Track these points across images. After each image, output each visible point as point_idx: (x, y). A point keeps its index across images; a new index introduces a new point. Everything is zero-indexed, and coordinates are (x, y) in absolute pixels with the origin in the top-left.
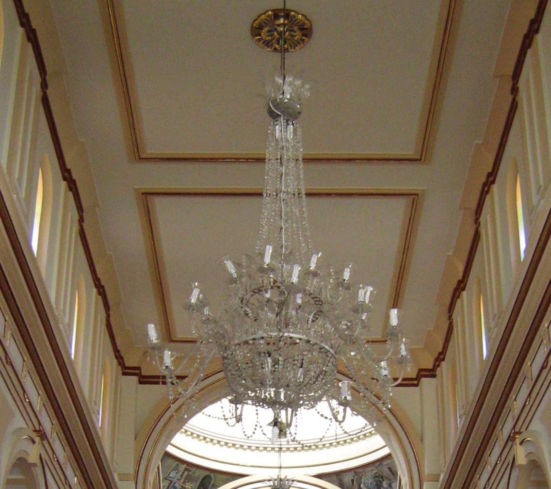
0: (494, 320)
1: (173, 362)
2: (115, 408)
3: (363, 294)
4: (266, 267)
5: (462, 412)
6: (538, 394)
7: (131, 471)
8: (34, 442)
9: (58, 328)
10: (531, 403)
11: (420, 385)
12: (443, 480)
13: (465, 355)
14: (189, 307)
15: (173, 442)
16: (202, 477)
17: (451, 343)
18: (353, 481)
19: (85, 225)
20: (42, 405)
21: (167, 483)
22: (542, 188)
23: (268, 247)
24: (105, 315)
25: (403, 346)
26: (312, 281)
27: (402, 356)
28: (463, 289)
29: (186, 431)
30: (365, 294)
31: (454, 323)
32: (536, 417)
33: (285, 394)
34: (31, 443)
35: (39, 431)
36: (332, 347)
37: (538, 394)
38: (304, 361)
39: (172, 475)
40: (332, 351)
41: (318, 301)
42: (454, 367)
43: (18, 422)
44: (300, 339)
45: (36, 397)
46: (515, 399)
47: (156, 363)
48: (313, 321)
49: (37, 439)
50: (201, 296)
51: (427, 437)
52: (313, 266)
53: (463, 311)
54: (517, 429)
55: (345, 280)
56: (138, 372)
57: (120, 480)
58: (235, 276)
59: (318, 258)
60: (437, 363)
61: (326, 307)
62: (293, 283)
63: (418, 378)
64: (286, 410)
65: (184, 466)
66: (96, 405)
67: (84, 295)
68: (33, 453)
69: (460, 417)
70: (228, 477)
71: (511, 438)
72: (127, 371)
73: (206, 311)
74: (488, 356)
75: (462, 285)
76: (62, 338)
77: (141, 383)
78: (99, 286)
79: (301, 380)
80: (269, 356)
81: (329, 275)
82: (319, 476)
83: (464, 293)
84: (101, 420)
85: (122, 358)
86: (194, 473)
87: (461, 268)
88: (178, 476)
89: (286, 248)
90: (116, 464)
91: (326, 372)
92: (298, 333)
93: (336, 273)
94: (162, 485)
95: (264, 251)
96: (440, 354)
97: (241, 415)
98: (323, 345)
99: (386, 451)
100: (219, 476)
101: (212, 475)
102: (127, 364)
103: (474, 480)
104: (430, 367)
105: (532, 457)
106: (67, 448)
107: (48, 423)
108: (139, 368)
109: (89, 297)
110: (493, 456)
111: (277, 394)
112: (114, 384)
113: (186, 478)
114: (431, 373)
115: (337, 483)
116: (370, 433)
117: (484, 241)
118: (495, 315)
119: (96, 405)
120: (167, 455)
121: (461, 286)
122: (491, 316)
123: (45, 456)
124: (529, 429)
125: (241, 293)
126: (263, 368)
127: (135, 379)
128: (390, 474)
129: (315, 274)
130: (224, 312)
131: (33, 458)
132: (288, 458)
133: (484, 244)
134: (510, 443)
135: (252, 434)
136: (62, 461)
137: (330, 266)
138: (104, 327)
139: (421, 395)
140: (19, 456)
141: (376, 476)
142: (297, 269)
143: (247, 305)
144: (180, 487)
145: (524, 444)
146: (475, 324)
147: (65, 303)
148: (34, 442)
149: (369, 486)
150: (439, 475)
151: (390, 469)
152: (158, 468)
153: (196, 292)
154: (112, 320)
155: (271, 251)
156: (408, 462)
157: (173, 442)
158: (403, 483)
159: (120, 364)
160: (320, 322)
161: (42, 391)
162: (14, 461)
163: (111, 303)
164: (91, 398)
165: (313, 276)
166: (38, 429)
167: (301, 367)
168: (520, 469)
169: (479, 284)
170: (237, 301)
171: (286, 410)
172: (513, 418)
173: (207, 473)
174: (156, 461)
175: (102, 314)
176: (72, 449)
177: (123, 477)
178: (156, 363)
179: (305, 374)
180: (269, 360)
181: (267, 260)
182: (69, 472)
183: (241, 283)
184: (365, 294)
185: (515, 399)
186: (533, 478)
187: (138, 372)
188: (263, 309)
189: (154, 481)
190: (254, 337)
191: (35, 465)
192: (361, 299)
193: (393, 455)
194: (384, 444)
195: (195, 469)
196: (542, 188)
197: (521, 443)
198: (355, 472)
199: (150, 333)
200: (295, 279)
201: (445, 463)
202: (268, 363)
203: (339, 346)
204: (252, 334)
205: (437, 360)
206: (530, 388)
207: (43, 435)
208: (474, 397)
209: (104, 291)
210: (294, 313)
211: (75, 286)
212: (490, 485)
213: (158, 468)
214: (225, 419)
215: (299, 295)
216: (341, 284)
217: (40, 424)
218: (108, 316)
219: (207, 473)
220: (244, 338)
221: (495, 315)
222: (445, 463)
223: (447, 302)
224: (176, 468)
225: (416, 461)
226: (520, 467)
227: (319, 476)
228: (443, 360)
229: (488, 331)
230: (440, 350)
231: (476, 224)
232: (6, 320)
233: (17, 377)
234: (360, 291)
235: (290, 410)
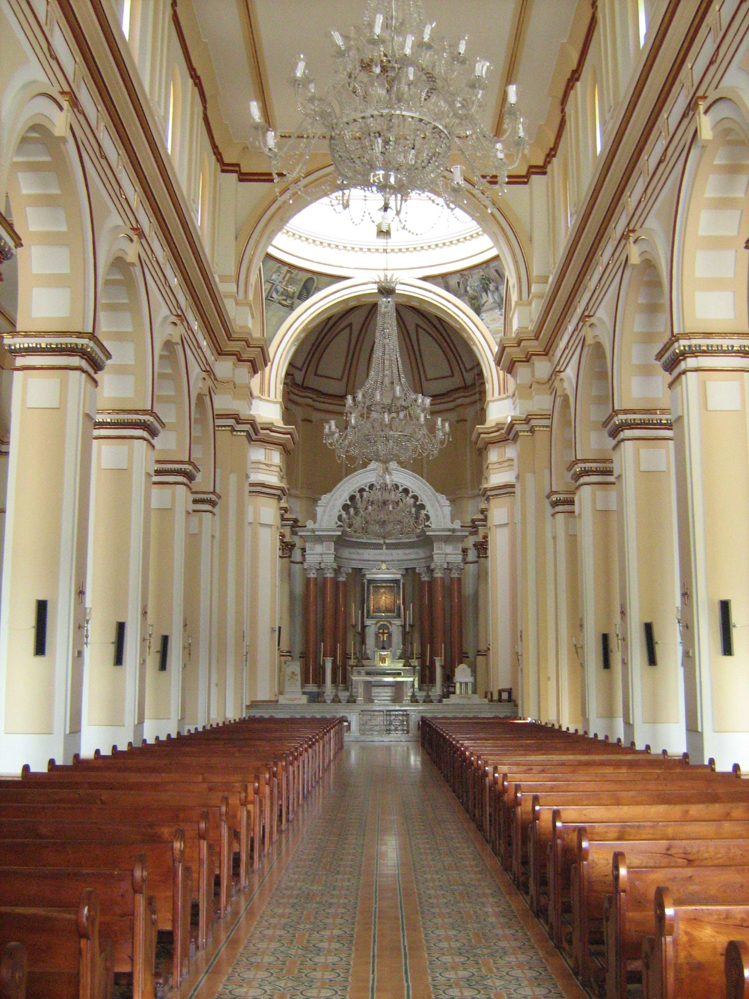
0: (609, 112)
1: (277, 145)
2: (215, 198)
3: (480, 68)
4: (376, 38)
5: (573, 210)
6: (659, 180)
7: (232, 270)
8: (132, 240)
9: (154, 120)
10: (646, 201)
11: (530, 182)
12: (491, 437)
13: (578, 147)
14: (295, 82)
15: (274, 242)
16: (304, 279)
17: (563, 139)
18: (459, 283)
19: (178, 10)
20: (139, 202)
21: (268, 286)
22: (613, 108)
23: (378, 16)
24: (201, 108)
25: (521, 126)
26: (426, 54)
27: (520, 137)
28: (578, 80)
29: (288, 232)
30: (482, 68)
31: (567, 118)
32: (653, 212)
33: (396, 177)
34: (130, 242)
35: (137, 229)
36: (446, 127)
37: (659, 180)
38: (416, 142)
39: (274, 277)
40: (445, 131)
41: (431, 78)
42: (566, 161)
43: (115, 219)
44: (412, 118)
45: (133, 193)
46: (630, 196)
47: (259, 143)
48: (425, 99)
49: (135, 238)
50: (307, 71)
51: (536, 238)
52: (426, 38)
53: (576, 104)
54: (631, 228)
55: (460, 53)
56: (237, 169)
57: (221, 282)
58: (343, 48)
59: (432, 28)
60: (548, 159)
61: (439, 83)
62: (406, 55)
63: (527, 176)
64: (396, 197)
65: (286, 268)
66: (194, 202)
67: (179, 87)
68: (132, 252)
69: (571, 216)
70: (334, 279)
71: (624, 237)
72: (226, 167)
73: (312, 88)
74: (646, 44)
75: (576, 76)
76: (158, 131)
77: (241, 180)
78: (194, 77)
79: (413, 162)
80: (380, 136)
81: (444, 50)
82: (425, 279)
83: (578, 84)
84: (200, 219)
85: (220, 154)
86: (296, 275)
87: (575, 57)
88: (280, 279)
89: (397, 19)
90: (217, 265)
91: (439, 154)
92: (411, 111)
93: (450, 46)
94: (263, 288)
95: (374, 21)
96: (551, 149)
97: (348, 201)
98: (437, 124)
99: (494, 252)
100: (323, 279)
101: (315, 277)
102: (227, 160)
103: (585, 282)
104: (541, 163)
105: (648, 256)
106: (167, 248)
107: (146, 222)
108: (238, 165)
109: (184, 92)
110: (605, 255)
111: (387, 177)
112: (212, 179)
113: (288, 281)
114: (542, 170)
115: (442, 285)
116: (477, 234)
117: (601, 29)
118: (611, 107)
119: (194, 202)
120: (269, 256)
121: (575, 76)
122: (607, 108)
123: (143, 256)
124: (644, 226)
125: (349, 67)
126: (372, 150)
127: (234, 176)
128: (497, 276)
129: (429, 47)
130: (332, 88)
131: (131, 258)
132: (394, 261)
133: (601, 32)
134: (623, 242)
135: (360, 221)
136: (161, 261)
137: (443, 38)
138: (201, 120)
139: (531, 193)
140: (116, 255)
141: (483, 279)
142: (410, 40)
143: (354, 81)
144: (282, 290)
145: (638, 243)
146: (589, 113)
147: (160, 95)
148: (132, 240)
149: (476, 288)
150: (548, 277)
151: (497, 271)
152: (260, 271)
153: (301, 66)
154: (209, 113)
155: (381, 21)
156: (516, 263)
157: (274, 243)
158: (511, 284)
159: (218, 160)
160: (434, 99)
161: (138, 188)
162: (112, 260)
163: (207, 95)
164: (189, 195)
165: (426, 49)
166: (135, 226)
167: (413, 148)
168: (633, 269)
169: (595, 72)
170: (344, 76)
171: (396, 197)
172: (628, 215)
173: (310, 275)
174: (258, 263)
175: (199, 108)
176: (171, 249)
177: (223, 279)
178: (259, 143)
179: (417, 157)
180: (380, 140)
181: (378, 30)
182: (169, 273)
183: (349, 56)
184: (482, 68)
185: (630, 196)
186: (646, 278)
187: (237, 169)
188: (373, 85)
189: (256, 285)
190: (363, 115)
191: (133, 264)
192: (478, 73)
193: (502, 257)
194: (492, 244)
195: (297, 271)
196: (613, 108)
197: (635, 242)
198: (461, 274)
199: (252, 110)
200: (408, 51)
201: (555, 265)
202: (378, 143)
203: (453, 126)
204: (361, 112)
205: (548, 156)
206: (646, 183)
207: (141, 234)
208: (587, 195)
209: (200, 82)
210: (406, 89)
211: (170, 77)
212: (602, 285)
213: (260, 271)
214: (332, 205)
215: (411, 70)
216: (457, 58)
217: (137, 221)
218: (205, 108)
219: (310, 275)
220: (354, 115)
221: (611, 107)
222: (555, 265)
223: (560, 95)
224: (278, 270)
225: (524, 262)
226: (634, 266)
227: (425, 279)
228: (554, 156)
229: (603, 123)
230: (552, 146)
231: (593, 8)
232: (98, 111)
233: (112, 171)
234: (477, 65)
235: (399, 196)
